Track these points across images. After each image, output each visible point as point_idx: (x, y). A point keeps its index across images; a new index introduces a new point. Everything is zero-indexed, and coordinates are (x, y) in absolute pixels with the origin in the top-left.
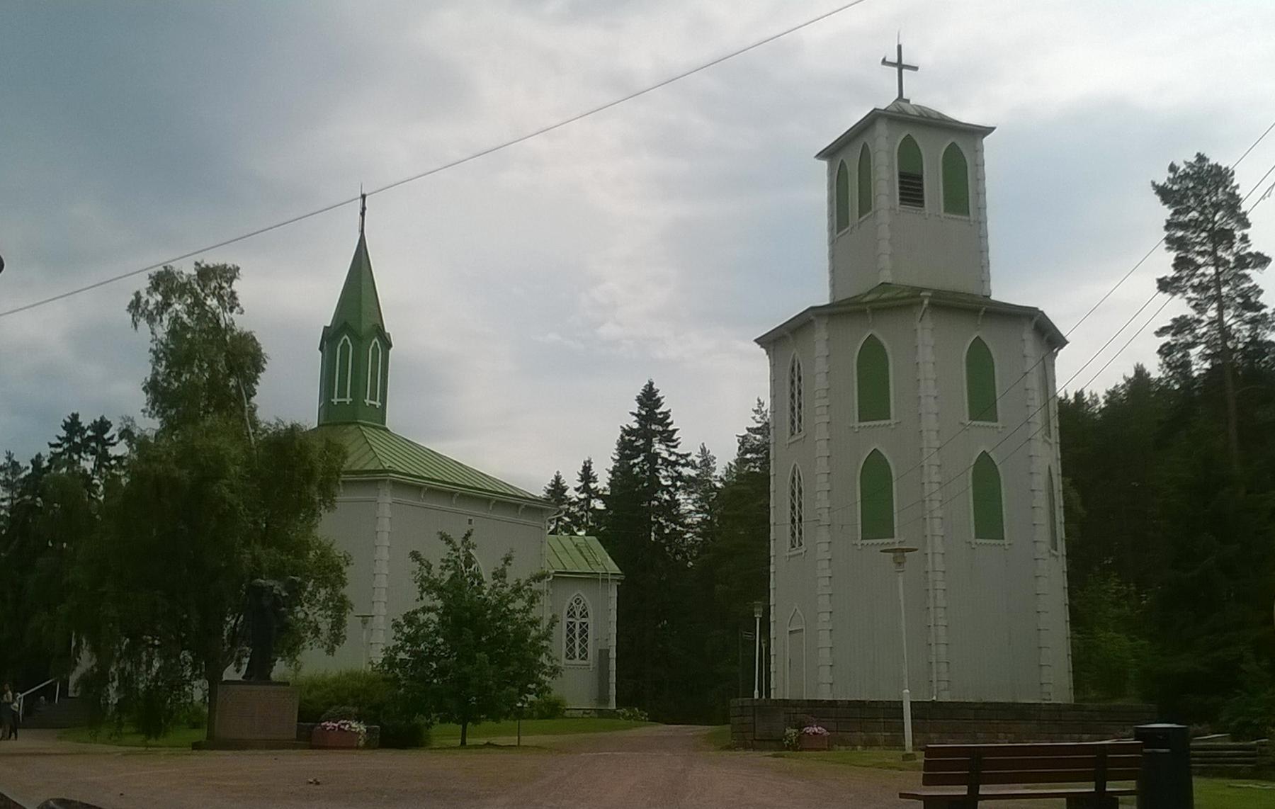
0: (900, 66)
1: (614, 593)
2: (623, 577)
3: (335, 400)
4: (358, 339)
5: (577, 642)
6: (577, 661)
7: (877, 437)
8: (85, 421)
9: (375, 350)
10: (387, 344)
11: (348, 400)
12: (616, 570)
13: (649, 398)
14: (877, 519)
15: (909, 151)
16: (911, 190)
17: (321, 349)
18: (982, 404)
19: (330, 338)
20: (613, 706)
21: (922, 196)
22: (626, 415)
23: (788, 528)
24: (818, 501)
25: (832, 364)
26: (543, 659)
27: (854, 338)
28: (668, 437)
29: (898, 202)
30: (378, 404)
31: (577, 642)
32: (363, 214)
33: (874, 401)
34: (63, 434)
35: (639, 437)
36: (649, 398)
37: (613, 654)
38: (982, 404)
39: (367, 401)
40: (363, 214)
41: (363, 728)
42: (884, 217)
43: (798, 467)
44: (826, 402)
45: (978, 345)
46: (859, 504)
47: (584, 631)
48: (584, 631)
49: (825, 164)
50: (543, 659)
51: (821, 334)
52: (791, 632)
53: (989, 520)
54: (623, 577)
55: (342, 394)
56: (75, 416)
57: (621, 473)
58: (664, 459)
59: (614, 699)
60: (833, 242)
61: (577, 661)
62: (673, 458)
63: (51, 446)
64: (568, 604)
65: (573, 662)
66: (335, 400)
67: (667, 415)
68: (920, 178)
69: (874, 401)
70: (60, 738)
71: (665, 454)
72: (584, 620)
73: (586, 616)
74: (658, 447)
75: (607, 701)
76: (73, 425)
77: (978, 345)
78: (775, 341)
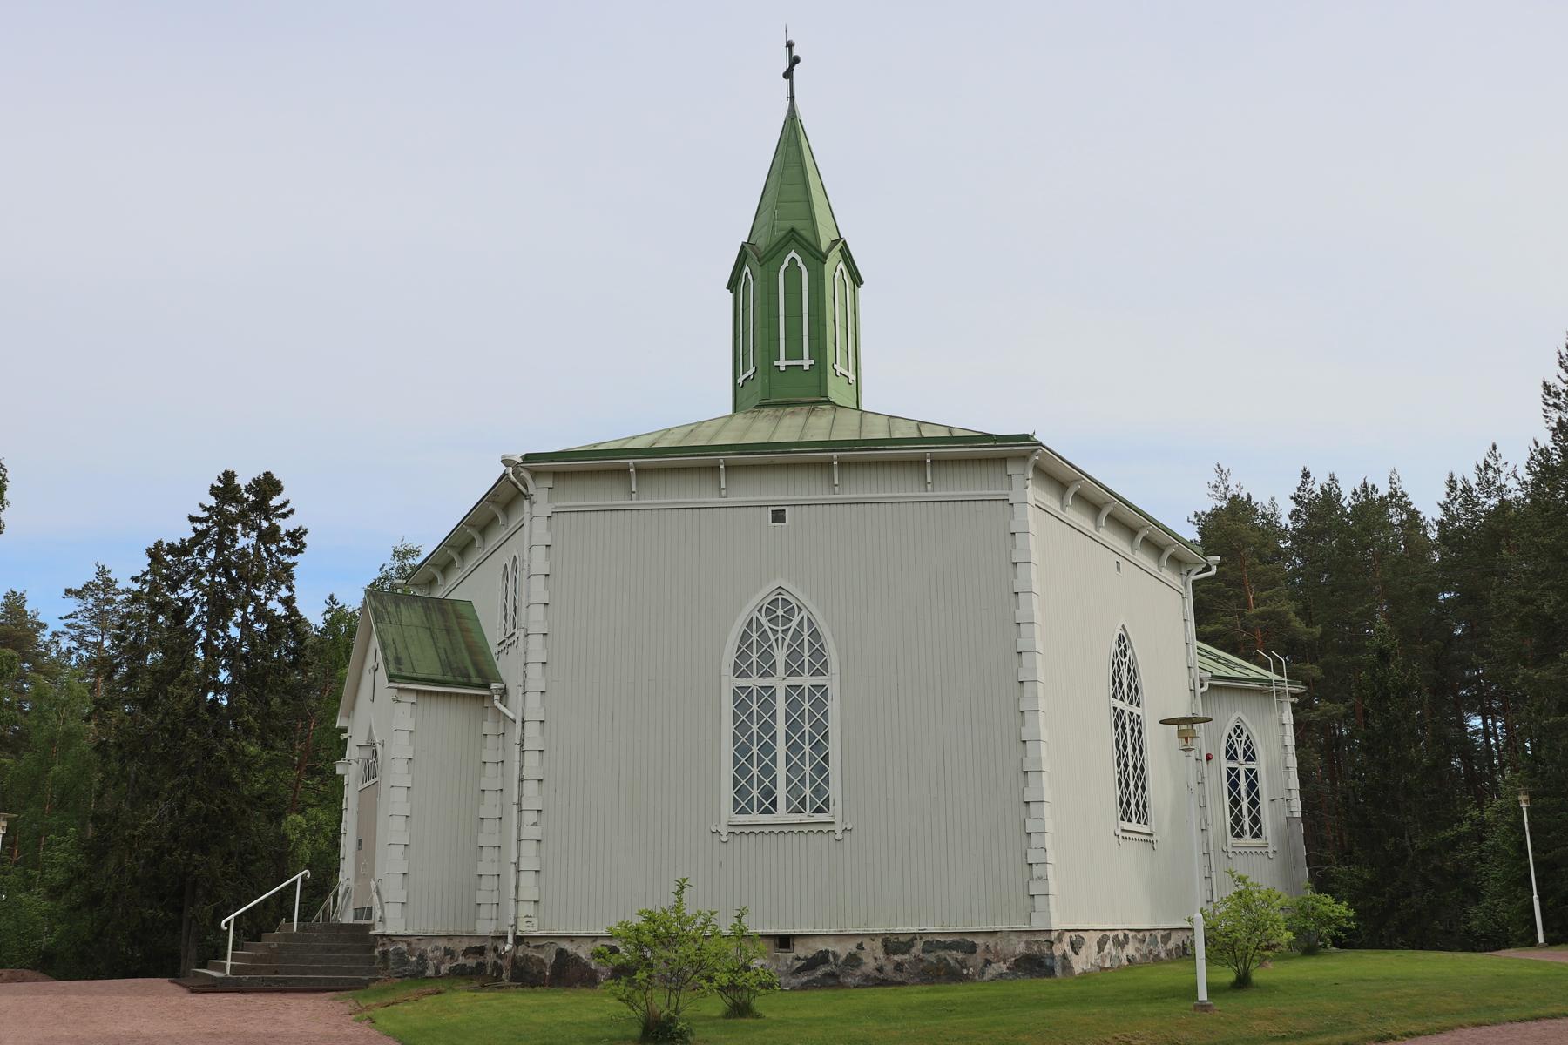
3: (782, 363)
4: (817, 257)
5: (1245, 804)
6: (1247, 839)
8: (243, 481)
10: (857, 280)
11: (807, 363)
17: (732, 285)
30: (807, 363)
31: (1245, 804)
34: (211, 501)
45: (781, 635)
47: (1252, 786)
48: (1252, 786)
55: (794, 352)
56: (228, 477)
61: (1247, 839)
63: (192, 519)
64: (1225, 737)
65: (1241, 842)
66: (782, 363)
70: (475, 990)
72: (1251, 765)
73: (1251, 758)
76: (226, 488)
77: (781, 635)
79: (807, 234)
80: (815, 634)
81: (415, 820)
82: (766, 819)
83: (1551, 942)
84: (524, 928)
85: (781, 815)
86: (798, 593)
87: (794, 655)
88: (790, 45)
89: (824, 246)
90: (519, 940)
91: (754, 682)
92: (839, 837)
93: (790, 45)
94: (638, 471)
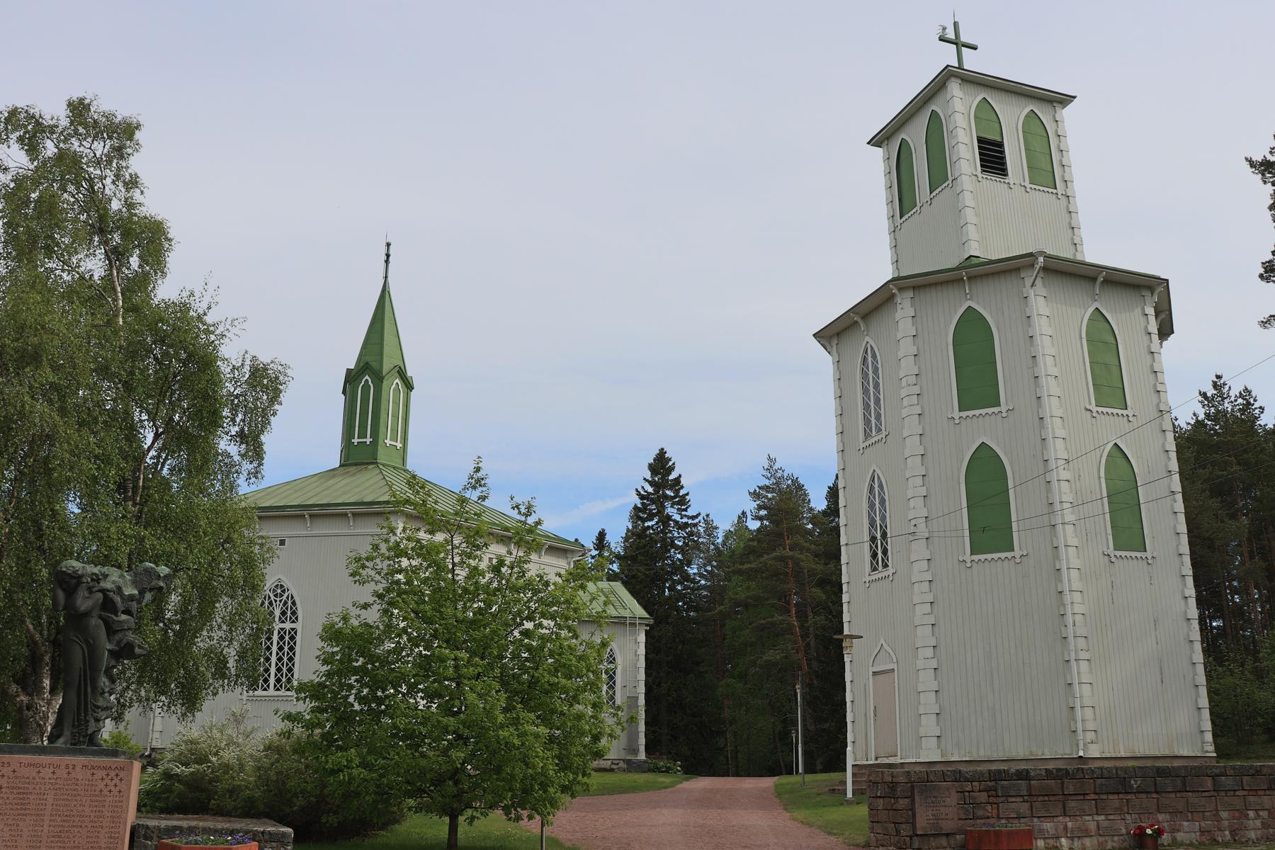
0: (957, 43)
1: (642, 638)
2: (652, 622)
3: (356, 441)
4: (379, 378)
7: (985, 428)
9: (397, 390)
10: (409, 386)
11: (368, 440)
12: (645, 614)
13: (661, 465)
14: (990, 524)
15: (985, 113)
16: (992, 158)
17: (344, 392)
18: (1109, 388)
19: (352, 378)
20: (642, 756)
21: (1004, 164)
22: (640, 476)
23: (867, 546)
24: (906, 511)
25: (918, 346)
26: (192, 313)
27: (946, 313)
28: (682, 502)
29: (979, 168)
30: (399, 445)
32: (387, 261)
33: (977, 380)
35: (653, 501)
36: (661, 465)
37: (642, 701)
38: (1109, 388)
39: (388, 442)
40: (387, 261)
41: (290, 830)
42: (967, 183)
43: (878, 471)
44: (916, 390)
46: (965, 511)
49: (879, 152)
50: (192, 313)
51: (904, 308)
52: (875, 673)
53: (1128, 531)
54: (652, 622)
57: (636, 537)
58: (676, 522)
59: (642, 748)
60: (894, 231)
62: (685, 520)
66: (356, 441)
67: (677, 480)
68: (1001, 145)
69: (977, 380)
71: (677, 517)
74: (671, 511)
75: (635, 751)
78: (838, 334)
79: (374, 365)
80: (294, 603)
81: (914, 689)
82: (265, 693)
83: (810, 769)
84: (155, 744)
85: (271, 692)
86: (287, 583)
87: (283, 613)
88: (388, 245)
89: (386, 369)
90: (153, 750)
91: (288, 626)
92: (1018, 560)
93: (388, 245)
94: (969, 278)
